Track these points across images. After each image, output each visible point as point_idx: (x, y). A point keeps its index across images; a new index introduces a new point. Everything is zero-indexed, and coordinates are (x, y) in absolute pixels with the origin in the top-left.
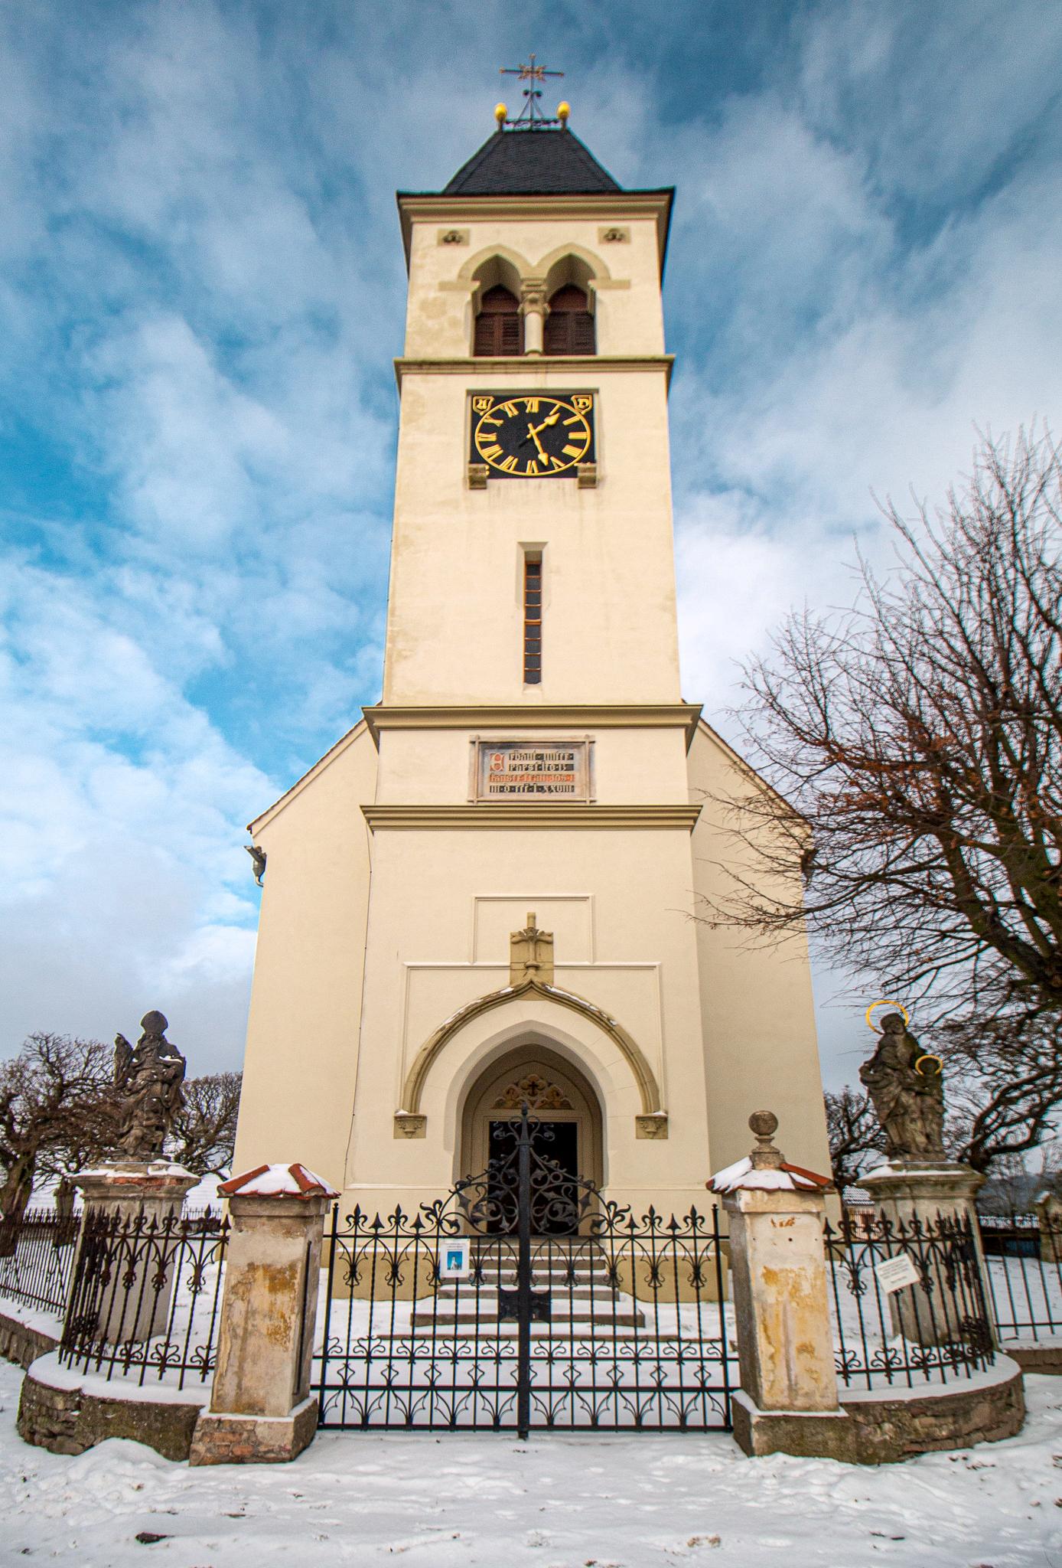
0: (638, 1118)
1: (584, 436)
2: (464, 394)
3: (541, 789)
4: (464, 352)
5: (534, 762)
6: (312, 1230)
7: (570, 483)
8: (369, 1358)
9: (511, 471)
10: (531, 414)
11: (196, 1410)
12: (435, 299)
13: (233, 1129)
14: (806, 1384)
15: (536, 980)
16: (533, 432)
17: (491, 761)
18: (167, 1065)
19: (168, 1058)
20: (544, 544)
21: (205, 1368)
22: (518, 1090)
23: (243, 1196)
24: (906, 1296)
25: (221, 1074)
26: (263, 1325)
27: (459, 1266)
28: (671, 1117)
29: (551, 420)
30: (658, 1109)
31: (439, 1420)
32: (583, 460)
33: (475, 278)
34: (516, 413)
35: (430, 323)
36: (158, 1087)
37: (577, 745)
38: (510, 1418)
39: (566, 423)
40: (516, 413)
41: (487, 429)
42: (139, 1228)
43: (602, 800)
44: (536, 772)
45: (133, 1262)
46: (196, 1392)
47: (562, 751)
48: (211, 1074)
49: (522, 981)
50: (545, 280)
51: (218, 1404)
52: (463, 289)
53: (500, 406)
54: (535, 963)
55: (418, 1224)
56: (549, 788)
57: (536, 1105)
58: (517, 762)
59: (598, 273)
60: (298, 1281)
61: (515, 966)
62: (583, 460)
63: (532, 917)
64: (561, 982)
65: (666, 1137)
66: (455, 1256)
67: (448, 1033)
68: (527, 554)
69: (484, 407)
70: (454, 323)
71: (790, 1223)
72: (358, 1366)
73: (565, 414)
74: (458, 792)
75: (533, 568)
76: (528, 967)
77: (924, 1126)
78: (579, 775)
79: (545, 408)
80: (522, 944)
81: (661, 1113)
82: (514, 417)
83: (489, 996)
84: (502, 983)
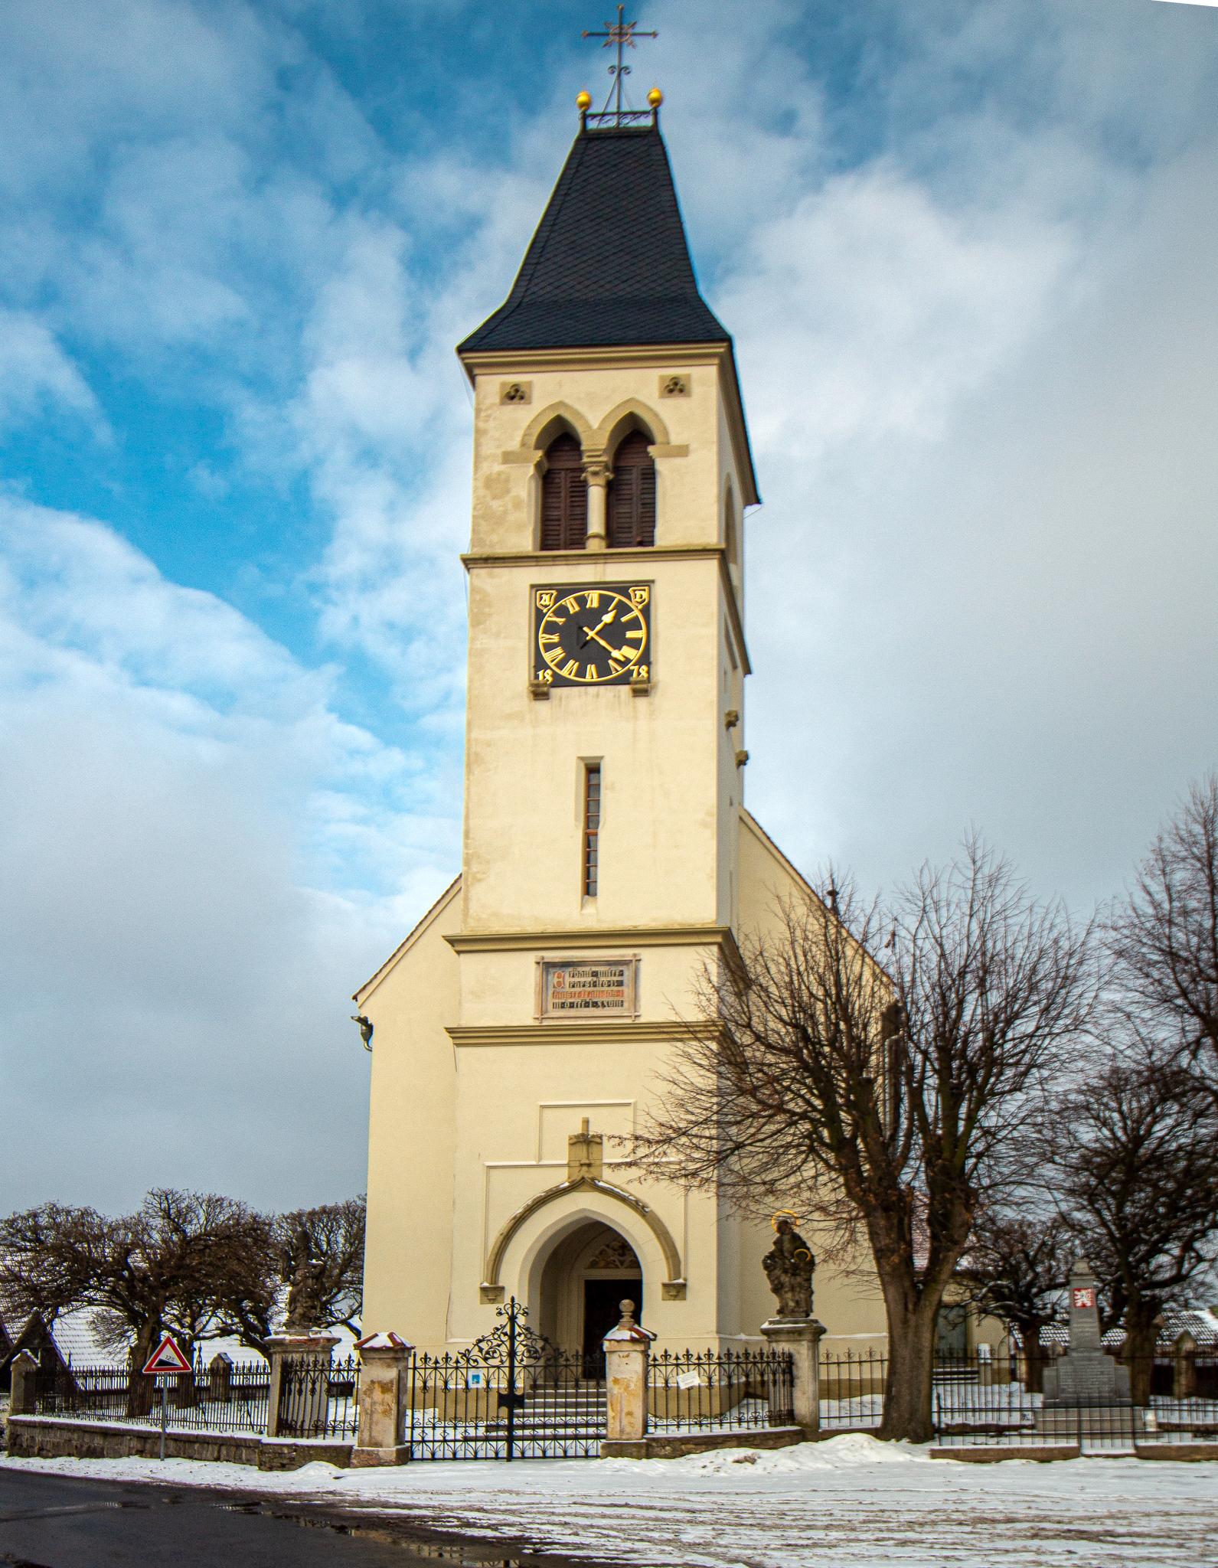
0: (664, 1285)
1: (640, 634)
2: (528, 589)
3: (595, 1005)
4: (526, 541)
5: (590, 979)
6: (401, 1365)
7: (625, 690)
8: (434, 1428)
9: (572, 677)
10: (591, 609)
11: (351, 1447)
12: (499, 474)
13: (360, 1268)
14: (628, 1429)
15: (587, 1176)
16: (591, 634)
17: (554, 979)
18: (315, 1266)
19: (314, 1261)
20: (602, 758)
21: (354, 1430)
22: (610, 1252)
23: (366, 1349)
24: (695, 1393)
25: (341, 1203)
26: (380, 1408)
27: (478, 1382)
28: (690, 1284)
29: (608, 618)
30: (679, 1277)
31: (469, 1455)
32: (639, 663)
33: (537, 447)
34: (577, 609)
35: (496, 505)
36: (310, 1281)
37: (627, 963)
38: (503, 1453)
39: (624, 619)
40: (577, 609)
41: (551, 628)
42: (315, 1366)
43: (645, 1019)
44: (592, 989)
45: (314, 1383)
46: (351, 1440)
47: (613, 968)
48: (330, 1204)
49: (577, 1177)
50: (605, 450)
51: (361, 1443)
52: (526, 460)
53: (562, 602)
54: (587, 1162)
55: (457, 1362)
56: (603, 1003)
57: (626, 1264)
58: (576, 979)
59: (658, 437)
60: (394, 1388)
61: (572, 1164)
62: (639, 663)
63: (586, 1122)
64: (609, 1178)
65: (684, 1299)
66: (476, 1377)
67: (519, 1221)
68: (586, 765)
69: (547, 603)
70: (517, 505)
71: (628, 1356)
72: (429, 1431)
73: (623, 609)
74: (523, 1012)
75: (593, 770)
76: (582, 1165)
77: (794, 1295)
78: (627, 990)
79: (605, 601)
80: (578, 1145)
81: (681, 1281)
82: (576, 613)
83: (551, 1190)
84: (562, 1179)
